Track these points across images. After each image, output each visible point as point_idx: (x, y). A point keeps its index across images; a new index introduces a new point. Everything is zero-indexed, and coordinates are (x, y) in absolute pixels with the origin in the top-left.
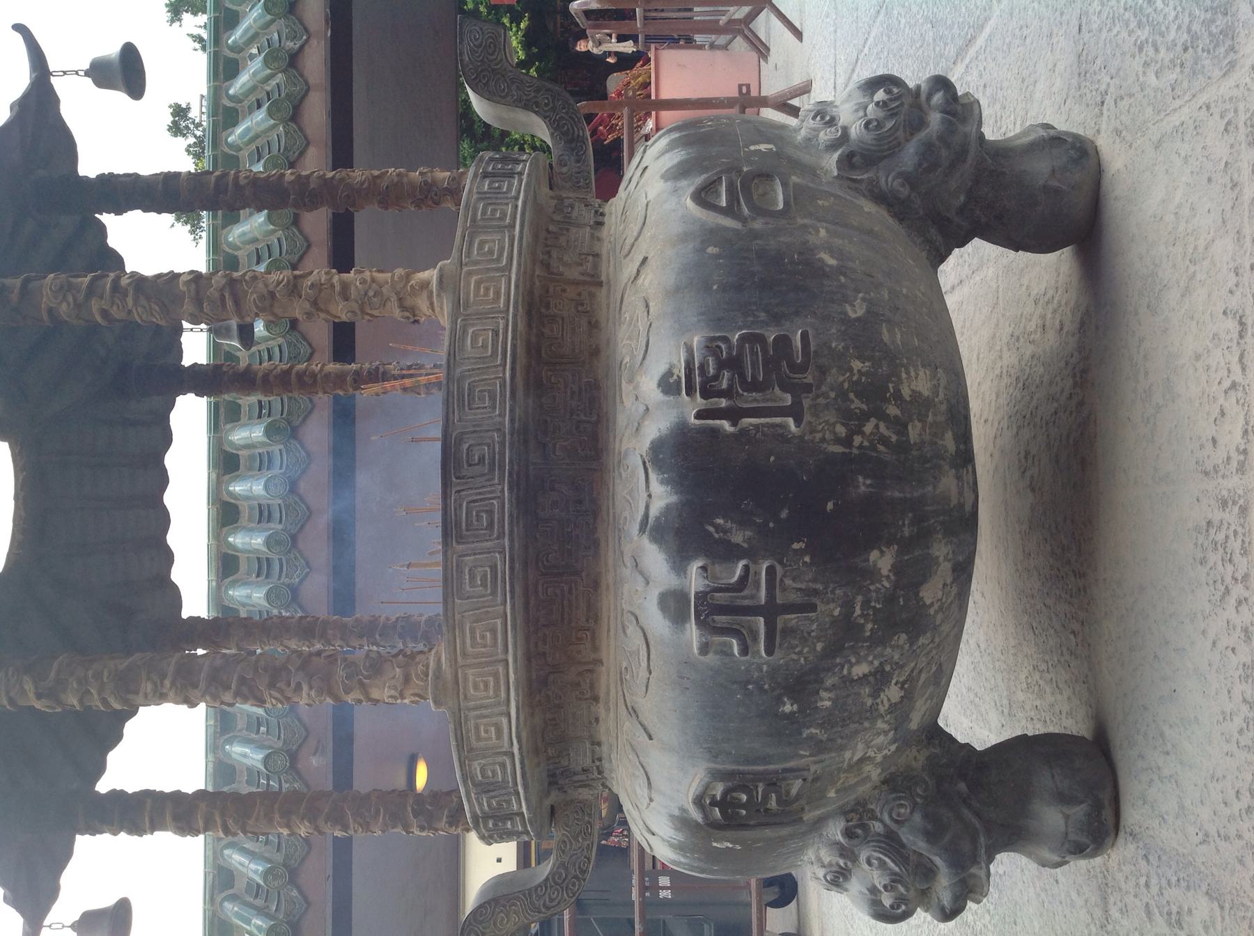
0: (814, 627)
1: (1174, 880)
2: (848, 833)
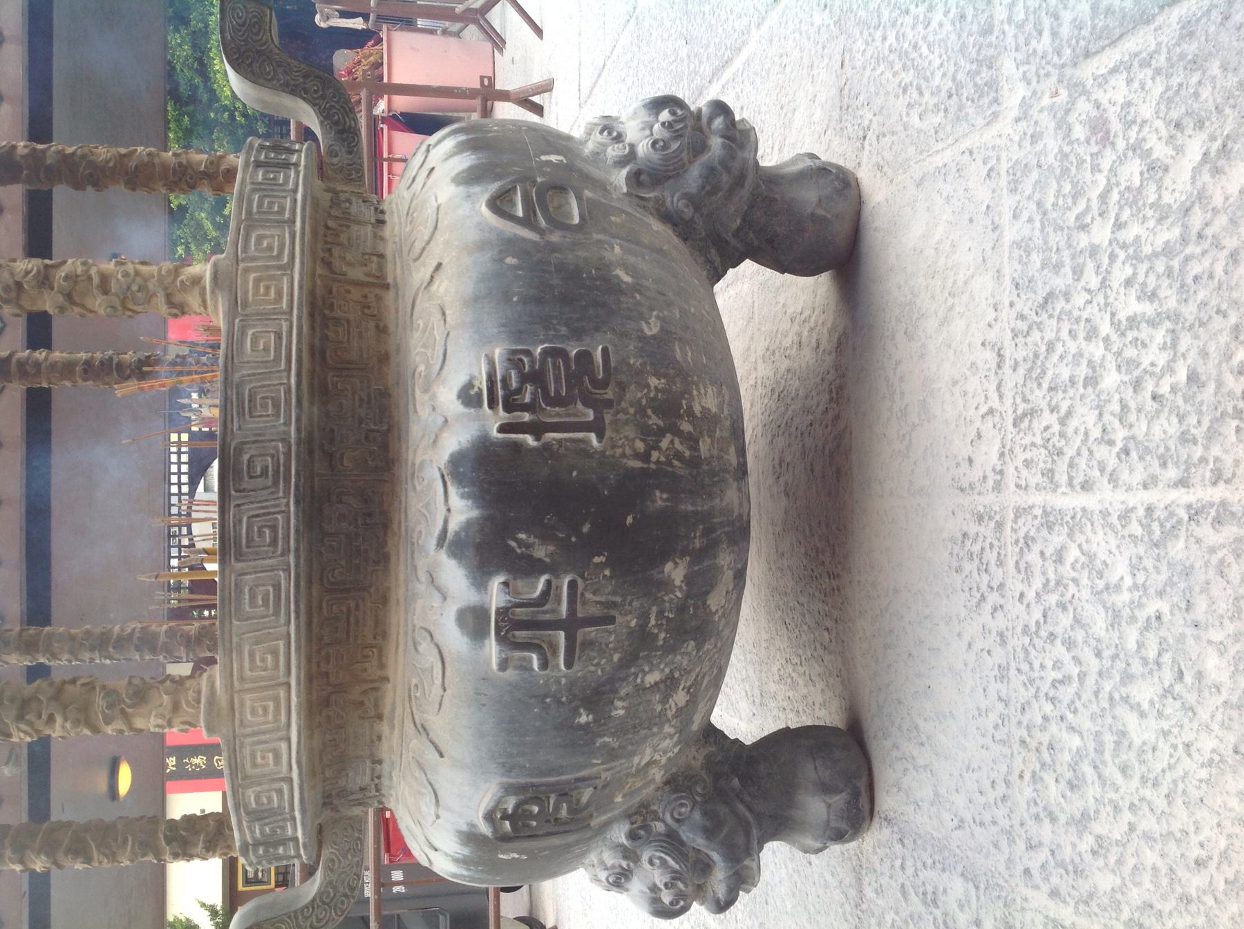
0: (612, 638)
1: (929, 862)
2: (632, 836)
